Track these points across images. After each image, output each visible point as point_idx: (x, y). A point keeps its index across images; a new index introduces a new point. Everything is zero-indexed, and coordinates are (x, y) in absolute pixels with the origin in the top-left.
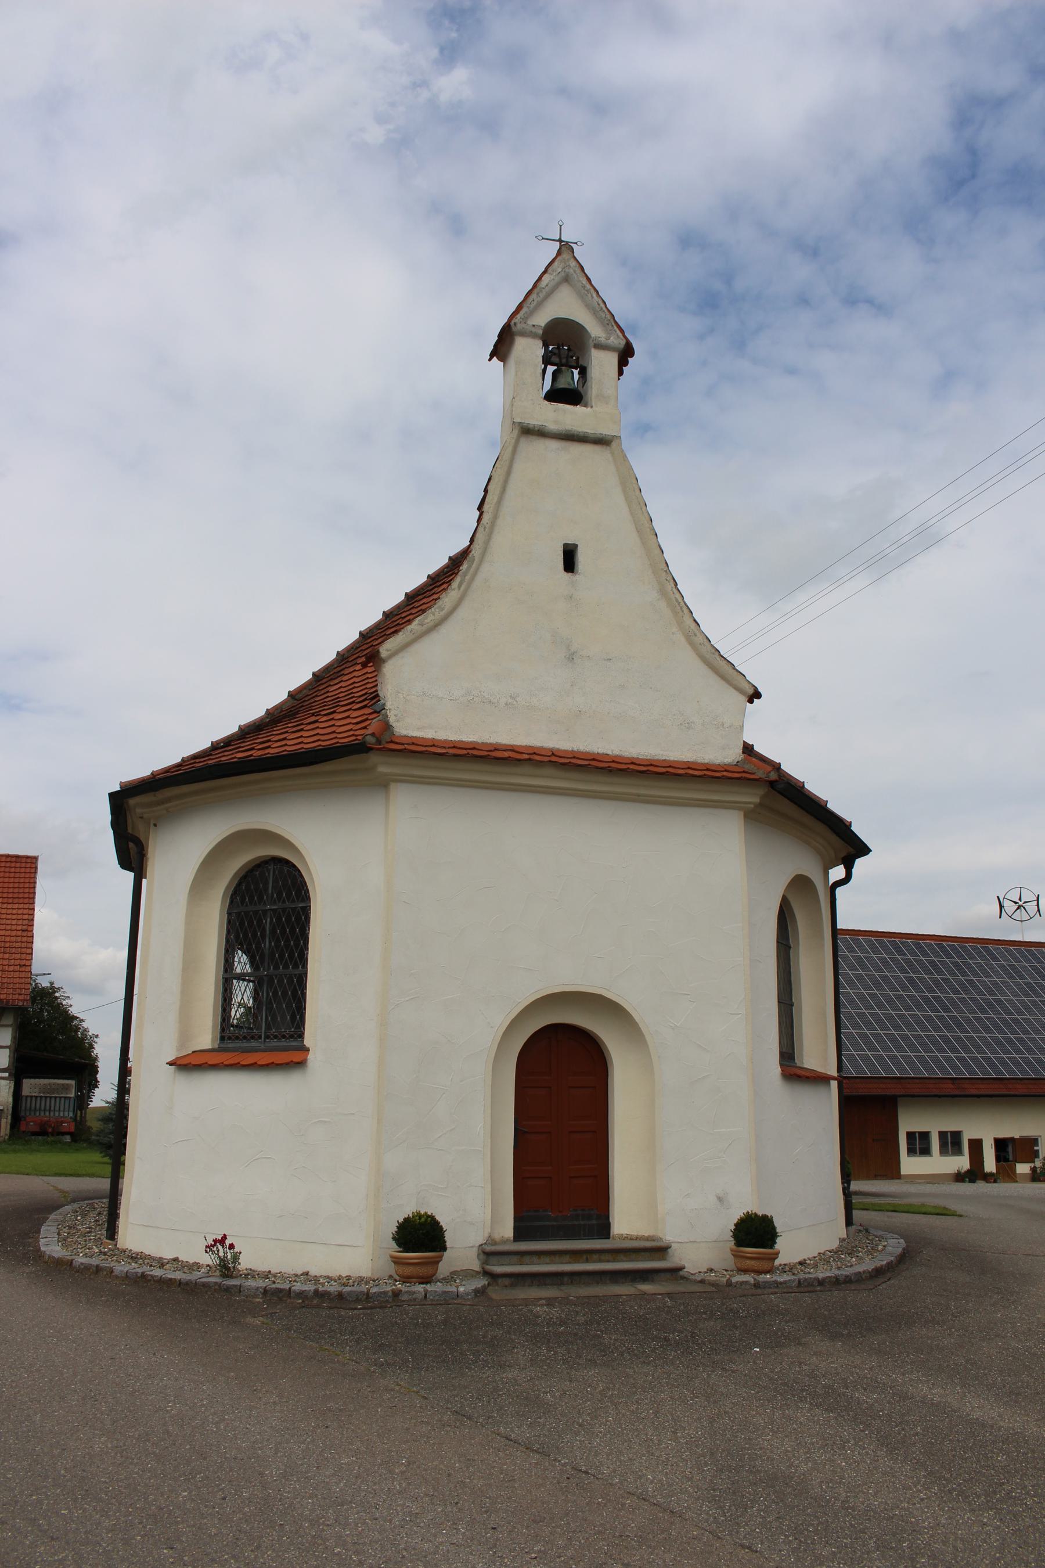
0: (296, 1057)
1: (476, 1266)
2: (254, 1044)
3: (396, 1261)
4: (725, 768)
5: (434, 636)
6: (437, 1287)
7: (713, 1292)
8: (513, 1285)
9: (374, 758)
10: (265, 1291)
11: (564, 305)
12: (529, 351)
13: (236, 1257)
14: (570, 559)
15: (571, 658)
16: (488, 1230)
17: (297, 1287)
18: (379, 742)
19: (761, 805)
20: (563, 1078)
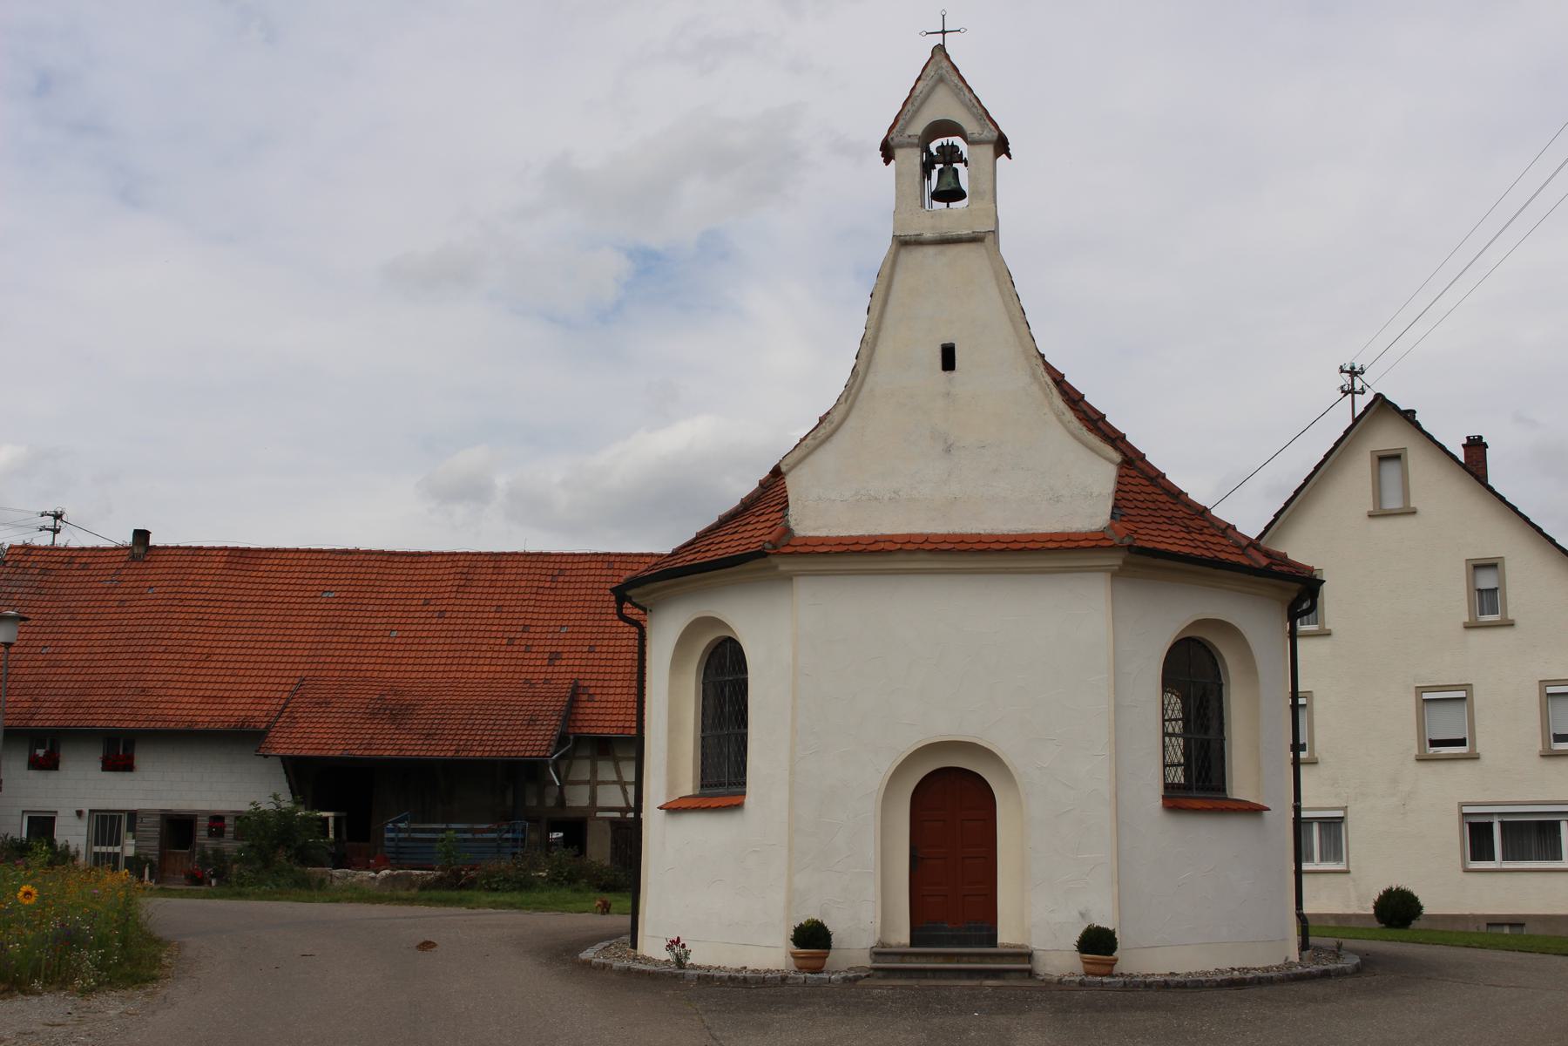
0: (735, 801)
1: (868, 963)
2: (721, 790)
3: (794, 955)
4: (1086, 536)
5: (828, 446)
6: (825, 976)
7: (1058, 992)
8: (885, 977)
9: (775, 560)
10: (699, 977)
11: (944, 107)
12: (911, 159)
13: (687, 953)
14: (948, 358)
15: (948, 450)
16: (878, 936)
17: (717, 974)
18: (775, 547)
19: (1125, 563)
20: (951, 813)
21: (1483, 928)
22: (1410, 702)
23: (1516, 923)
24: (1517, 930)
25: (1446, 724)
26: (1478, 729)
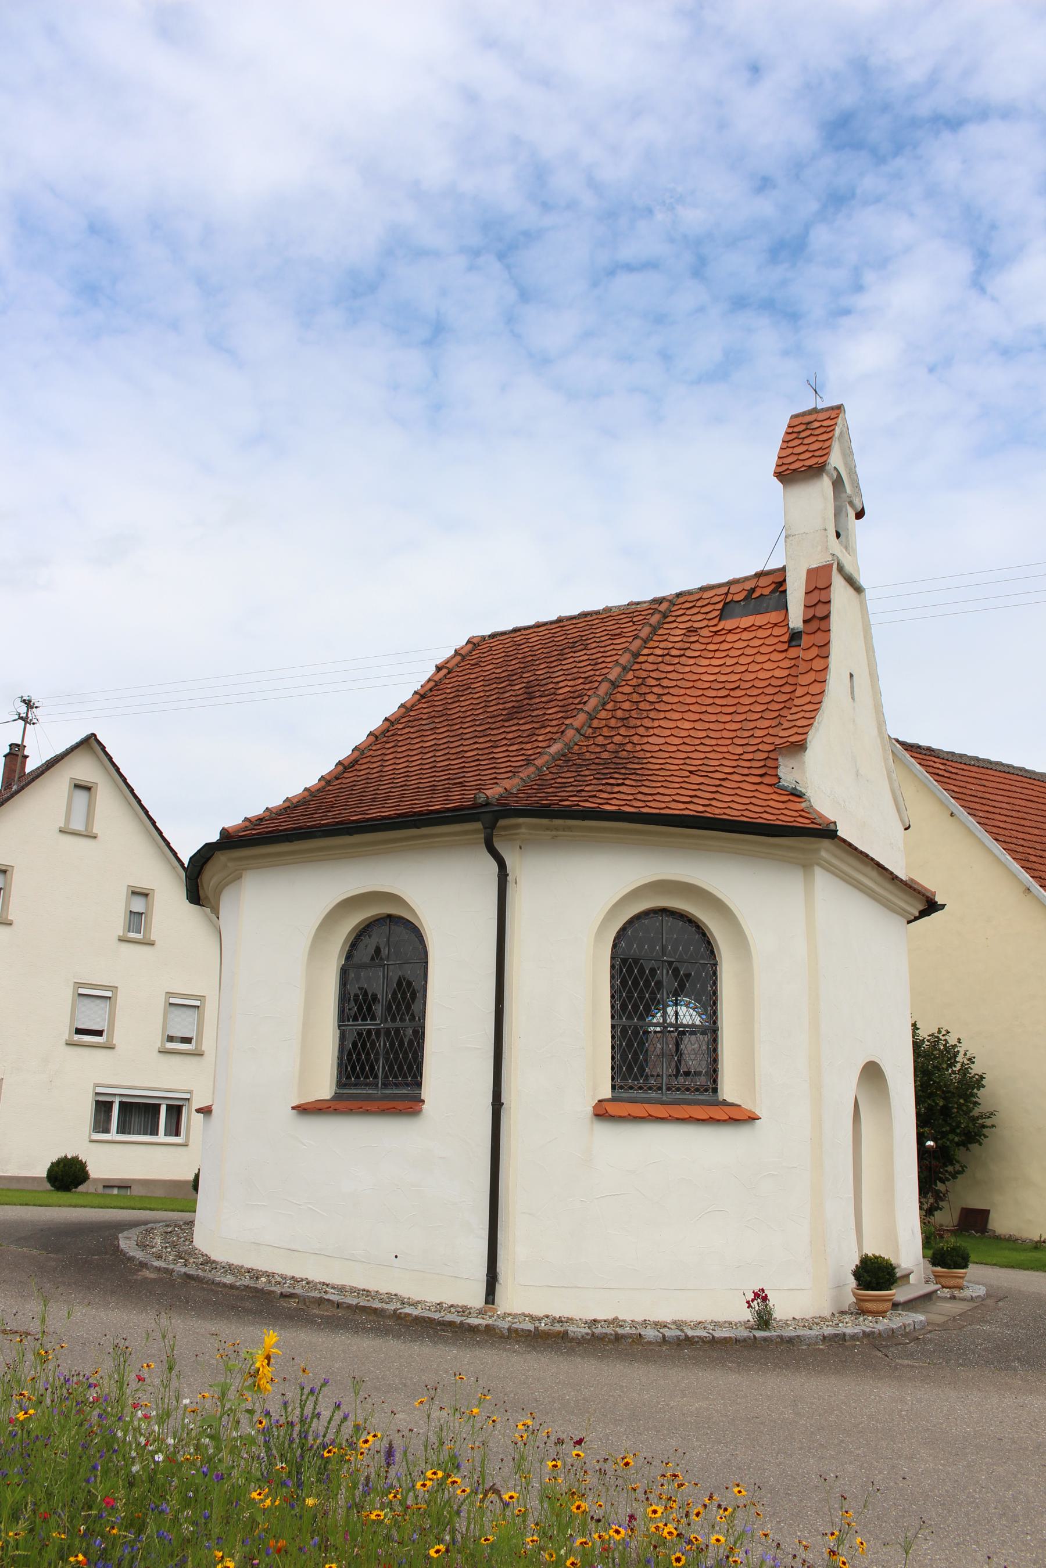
21: (100, 1190)
22: (68, 994)
23: (124, 1186)
24: (123, 1192)
25: (92, 1017)
26: (117, 1024)
